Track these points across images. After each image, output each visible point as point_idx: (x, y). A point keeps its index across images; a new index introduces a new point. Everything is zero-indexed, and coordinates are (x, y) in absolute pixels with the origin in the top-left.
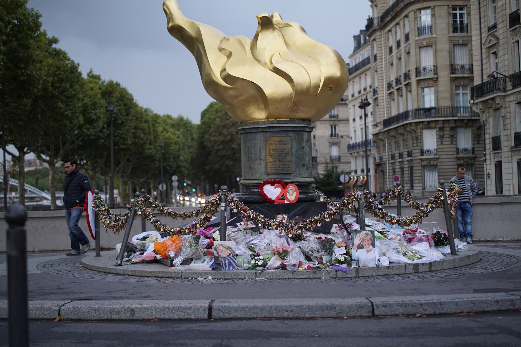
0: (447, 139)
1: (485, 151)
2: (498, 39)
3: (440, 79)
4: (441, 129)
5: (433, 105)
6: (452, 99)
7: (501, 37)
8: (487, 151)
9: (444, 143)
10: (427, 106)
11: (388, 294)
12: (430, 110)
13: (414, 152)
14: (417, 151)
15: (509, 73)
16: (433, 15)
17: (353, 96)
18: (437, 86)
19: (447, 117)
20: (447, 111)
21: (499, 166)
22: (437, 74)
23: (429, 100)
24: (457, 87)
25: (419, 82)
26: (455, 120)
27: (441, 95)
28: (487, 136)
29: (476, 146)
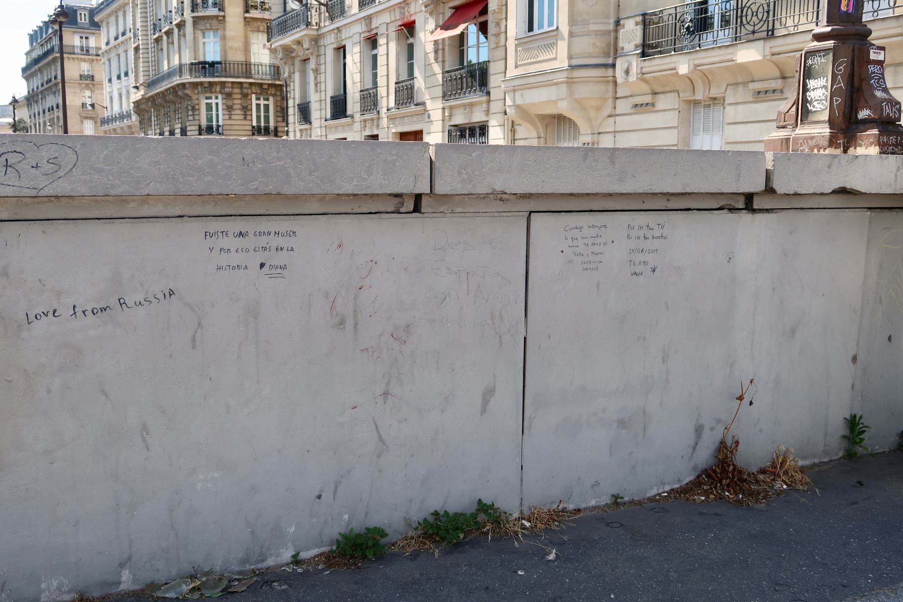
0: (239, 112)
1: (287, 126)
3: (227, 19)
4: (228, 96)
5: (218, 59)
8: (290, 126)
9: (233, 117)
10: (210, 58)
12: (212, 64)
13: (188, 128)
14: (193, 128)
17: (107, 44)
18: (225, 30)
19: (238, 77)
22: (223, 11)
25: (196, 21)
26: (251, 84)
27: (230, 44)
29: (280, 124)
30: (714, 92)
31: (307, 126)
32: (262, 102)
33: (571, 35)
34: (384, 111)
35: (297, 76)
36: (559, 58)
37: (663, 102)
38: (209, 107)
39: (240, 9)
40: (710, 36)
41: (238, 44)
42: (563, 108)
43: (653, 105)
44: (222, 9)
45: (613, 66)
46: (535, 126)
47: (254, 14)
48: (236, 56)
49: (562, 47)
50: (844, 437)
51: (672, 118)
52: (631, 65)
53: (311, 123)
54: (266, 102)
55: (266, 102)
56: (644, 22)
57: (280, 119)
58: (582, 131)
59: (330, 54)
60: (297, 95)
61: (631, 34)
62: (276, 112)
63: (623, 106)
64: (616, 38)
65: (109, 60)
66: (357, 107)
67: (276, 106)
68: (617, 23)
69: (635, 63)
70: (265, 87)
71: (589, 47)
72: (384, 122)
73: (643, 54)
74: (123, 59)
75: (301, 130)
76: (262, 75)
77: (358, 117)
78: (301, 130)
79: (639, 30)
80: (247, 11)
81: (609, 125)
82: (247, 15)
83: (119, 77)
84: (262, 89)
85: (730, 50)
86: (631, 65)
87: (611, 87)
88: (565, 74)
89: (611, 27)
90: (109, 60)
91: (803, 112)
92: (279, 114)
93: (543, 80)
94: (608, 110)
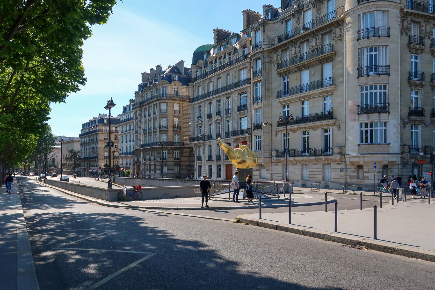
2: (202, 121)
4: (169, 150)
6: (173, 138)
7: (203, 121)
11: (182, 188)
15: (207, 134)
16: (167, 106)
20: (130, 137)
21: (200, 166)
23: (164, 138)
24: (175, 134)
25: (160, 131)
28: (195, 156)
34: (222, 160)
35: (197, 150)
37: (279, 164)
38: (163, 153)
39: (172, 128)
40: (338, 30)
41: (171, 137)
42: (263, 164)
44: (167, 129)
47: (175, 129)
48: (171, 140)
50: (159, 68)
51: (281, 167)
52: (274, 158)
59: (207, 147)
60: (197, 154)
61: (274, 153)
62: (180, 154)
63: (273, 164)
65: (123, 137)
66: (215, 158)
71: (267, 154)
72: (222, 162)
74: (128, 137)
76: (177, 145)
77: (215, 161)
81: (271, 167)
83: (127, 142)
84: (177, 148)
90: (123, 137)
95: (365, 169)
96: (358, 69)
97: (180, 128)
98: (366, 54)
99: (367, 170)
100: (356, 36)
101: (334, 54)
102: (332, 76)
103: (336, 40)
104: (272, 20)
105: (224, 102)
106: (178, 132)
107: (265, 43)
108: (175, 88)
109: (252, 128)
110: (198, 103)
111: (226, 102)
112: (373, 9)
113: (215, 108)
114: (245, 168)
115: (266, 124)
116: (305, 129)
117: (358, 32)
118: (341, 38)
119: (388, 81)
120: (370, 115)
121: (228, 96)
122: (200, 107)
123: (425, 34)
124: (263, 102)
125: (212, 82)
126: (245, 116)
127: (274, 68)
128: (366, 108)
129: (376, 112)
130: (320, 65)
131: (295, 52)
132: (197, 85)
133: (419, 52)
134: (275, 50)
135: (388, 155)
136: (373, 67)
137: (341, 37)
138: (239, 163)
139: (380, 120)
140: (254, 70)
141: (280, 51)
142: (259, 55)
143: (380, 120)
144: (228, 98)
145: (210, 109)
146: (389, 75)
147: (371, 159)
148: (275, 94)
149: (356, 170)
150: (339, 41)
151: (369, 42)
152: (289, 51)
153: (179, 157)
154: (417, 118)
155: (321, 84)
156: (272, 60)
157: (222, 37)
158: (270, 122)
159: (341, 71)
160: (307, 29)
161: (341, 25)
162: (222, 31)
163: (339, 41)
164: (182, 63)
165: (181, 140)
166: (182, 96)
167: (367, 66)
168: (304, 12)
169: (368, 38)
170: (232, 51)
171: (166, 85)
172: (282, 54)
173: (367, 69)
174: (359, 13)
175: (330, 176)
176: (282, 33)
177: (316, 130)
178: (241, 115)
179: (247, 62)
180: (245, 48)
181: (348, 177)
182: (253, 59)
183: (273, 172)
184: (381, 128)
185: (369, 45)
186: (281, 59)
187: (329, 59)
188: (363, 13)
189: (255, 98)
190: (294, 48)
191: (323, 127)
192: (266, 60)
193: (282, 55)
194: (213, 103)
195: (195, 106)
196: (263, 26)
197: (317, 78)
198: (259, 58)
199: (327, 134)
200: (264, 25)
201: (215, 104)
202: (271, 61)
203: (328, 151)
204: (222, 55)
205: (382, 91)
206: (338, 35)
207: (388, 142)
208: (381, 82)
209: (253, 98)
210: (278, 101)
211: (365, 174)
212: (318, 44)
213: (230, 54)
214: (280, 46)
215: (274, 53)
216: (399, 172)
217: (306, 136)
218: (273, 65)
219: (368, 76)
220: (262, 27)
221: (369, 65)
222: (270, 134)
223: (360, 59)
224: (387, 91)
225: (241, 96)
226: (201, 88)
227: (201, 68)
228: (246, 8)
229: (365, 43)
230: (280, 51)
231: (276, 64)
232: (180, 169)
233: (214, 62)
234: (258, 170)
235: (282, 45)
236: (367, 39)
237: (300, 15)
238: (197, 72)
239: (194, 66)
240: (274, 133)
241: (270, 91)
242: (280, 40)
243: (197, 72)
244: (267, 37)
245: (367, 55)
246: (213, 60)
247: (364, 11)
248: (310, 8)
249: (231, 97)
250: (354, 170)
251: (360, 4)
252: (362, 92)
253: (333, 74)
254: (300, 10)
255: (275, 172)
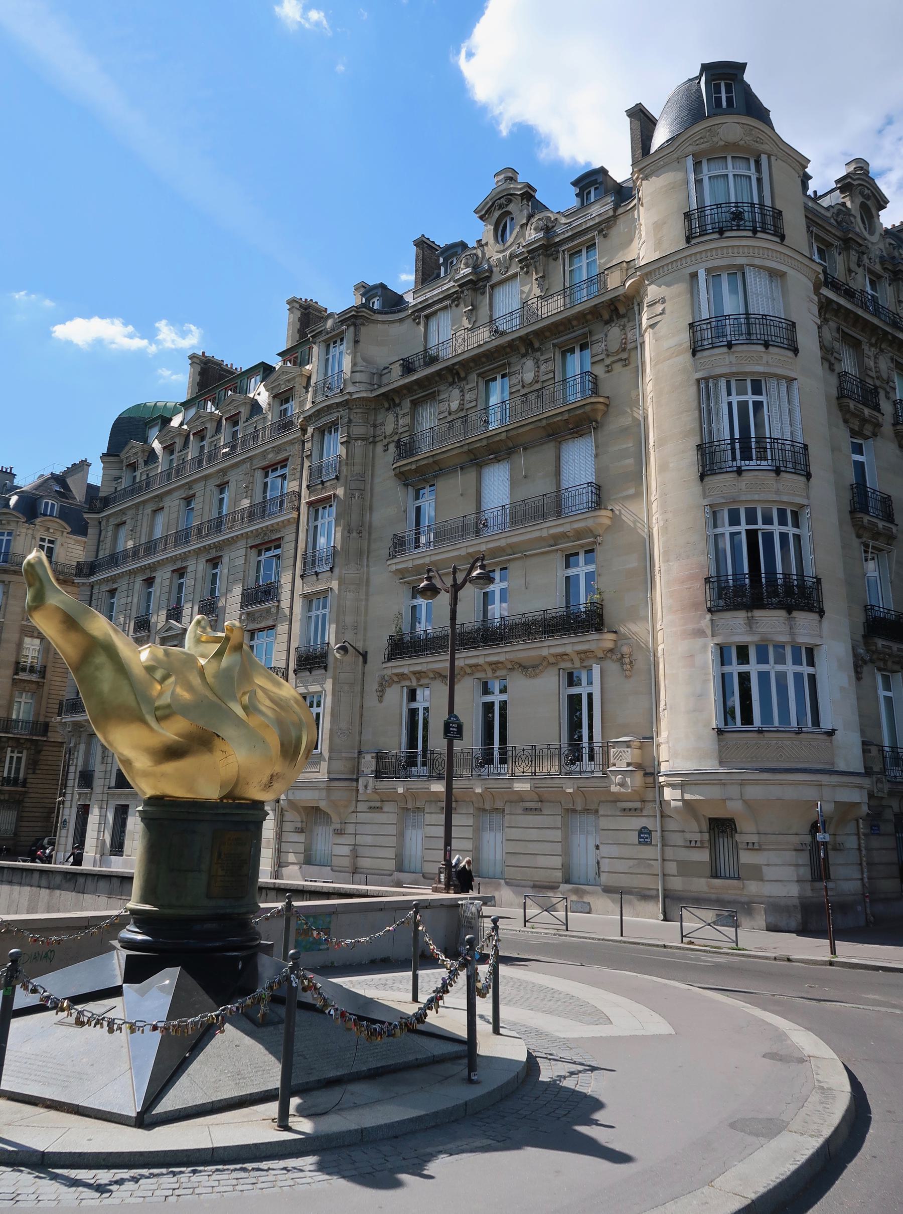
21: (84, 811)
29: (29, 776)
30: (418, 805)
31: (88, 791)
32: (16, 755)
33: (330, 758)
35: (82, 747)
36: (321, 773)
37: (388, 807)
40: (615, 332)
42: (323, 805)
43: (381, 808)
45: (357, 780)
46: (299, 812)
49: (324, 766)
51: (393, 818)
52: (368, 784)
53: (92, 789)
54: (20, 755)
55: (20, 755)
56: (377, 756)
57: (30, 771)
58: (333, 820)
60: (80, 762)
61: (369, 763)
63: (362, 807)
64: (359, 763)
67: (28, 759)
68: (360, 753)
69: (371, 782)
70: (22, 741)
73: (376, 777)
75: (80, 794)
76: (21, 733)
78: (80, 794)
79: (374, 761)
80: (17, 674)
82: (16, 677)
84: (18, 743)
85: (427, 783)
86: (368, 784)
87: (354, 794)
88: (325, 784)
89: (356, 755)
91: (440, 882)
92: (30, 766)
93: (311, 786)
94: (352, 809)
95: (747, 831)
96: (700, 447)
97: (43, 672)
98: (725, 399)
99: (754, 838)
100: (685, 337)
101: (601, 407)
102: (597, 477)
103: (608, 361)
104: (386, 313)
105: (200, 575)
106: (34, 686)
107: (358, 377)
108: (43, 540)
109: (292, 666)
110: (106, 580)
111: (204, 577)
112: (740, 261)
113: (165, 597)
114: (210, 792)
115: (343, 649)
116: (494, 671)
117: (691, 326)
118: (624, 355)
119: (808, 498)
120: (757, 613)
121: (213, 554)
122: (112, 592)
123: (878, 383)
124: (336, 570)
125: (166, 510)
126: (270, 623)
127: (385, 461)
128: (739, 589)
129: (779, 606)
130: (552, 445)
131: (462, 404)
132: (113, 521)
133: (868, 430)
134: (389, 400)
135: (834, 779)
136: (747, 445)
137: (628, 355)
138: (172, 752)
139: (792, 634)
140: (315, 461)
141: (407, 405)
142: (333, 417)
143: (792, 634)
144: (214, 562)
145: (149, 600)
146: (808, 476)
147: (775, 792)
148: (383, 546)
149: (706, 836)
150: (618, 367)
151: (733, 358)
152: (441, 401)
153: (21, 776)
154: (890, 648)
155: (554, 506)
156: (378, 432)
157: (211, 377)
158: (360, 646)
159: (630, 461)
160: (503, 333)
161: (623, 316)
162: (219, 364)
163: (618, 367)
164: (83, 466)
165: (37, 714)
166: (64, 565)
167: (732, 438)
168: (492, 287)
169: (730, 346)
170: (244, 411)
171: (12, 527)
172: (413, 414)
173: (733, 450)
174: (692, 270)
175: (592, 862)
176: (413, 349)
177: (536, 675)
178: (254, 620)
179: (291, 442)
180: (287, 401)
181: (672, 868)
182: (310, 430)
183: (360, 840)
184: (798, 669)
185: (734, 370)
186: (411, 427)
187: (581, 423)
188: (708, 271)
189: (310, 559)
190: (456, 392)
191: (563, 665)
192: (358, 430)
193: (413, 418)
194: (158, 580)
195: (95, 591)
196: (355, 325)
197: (541, 486)
198: (332, 427)
199: (582, 690)
200: (359, 322)
201: (167, 583)
202: (374, 437)
203: (585, 757)
204: (208, 425)
205: (790, 530)
206: (614, 346)
207: (826, 724)
208: (785, 498)
209: (305, 556)
210: (394, 568)
211: (746, 858)
212: (542, 378)
213: (234, 420)
214: (408, 388)
215: (388, 409)
216: (859, 849)
217: (496, 698)
218: (380, 448)
219: (739, 472)
220: (352, 329)
221: (737, 435)
222: (358, 689)
223: (705, 415)
224: (805, 532)
225: (259, 555)
226: (123, 532)
227: (133, 467)
228: (304, 295)
229: (720, 361)
230: (407, 405)
231: (392, 447)
232: (20, 819)
233: (177, 447)
234: (302, 832)
235: (416, 382)
236: (725, 350)
237: (480, 297)
238: (117, 478)
239: (112, 459)
240: (372, 686)
241: (365, 534)
242: (408, 367)
243: (117, 478)
244: (364, 360)
245: (730, 404)
246: (177, 440)
247: (710, 264)
248: (515, 276)
249: (225, 560)
250: (697, 837)
251: (693, 242)
252: (719, 530)
253: (598, 472)
254: (479, 280)
255: (369, 840)
